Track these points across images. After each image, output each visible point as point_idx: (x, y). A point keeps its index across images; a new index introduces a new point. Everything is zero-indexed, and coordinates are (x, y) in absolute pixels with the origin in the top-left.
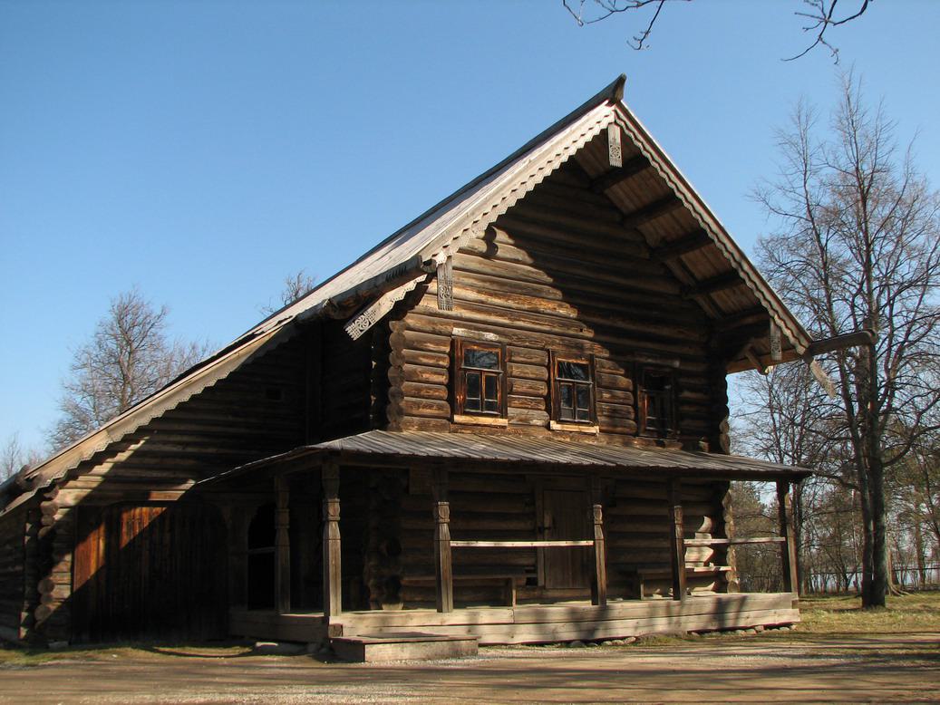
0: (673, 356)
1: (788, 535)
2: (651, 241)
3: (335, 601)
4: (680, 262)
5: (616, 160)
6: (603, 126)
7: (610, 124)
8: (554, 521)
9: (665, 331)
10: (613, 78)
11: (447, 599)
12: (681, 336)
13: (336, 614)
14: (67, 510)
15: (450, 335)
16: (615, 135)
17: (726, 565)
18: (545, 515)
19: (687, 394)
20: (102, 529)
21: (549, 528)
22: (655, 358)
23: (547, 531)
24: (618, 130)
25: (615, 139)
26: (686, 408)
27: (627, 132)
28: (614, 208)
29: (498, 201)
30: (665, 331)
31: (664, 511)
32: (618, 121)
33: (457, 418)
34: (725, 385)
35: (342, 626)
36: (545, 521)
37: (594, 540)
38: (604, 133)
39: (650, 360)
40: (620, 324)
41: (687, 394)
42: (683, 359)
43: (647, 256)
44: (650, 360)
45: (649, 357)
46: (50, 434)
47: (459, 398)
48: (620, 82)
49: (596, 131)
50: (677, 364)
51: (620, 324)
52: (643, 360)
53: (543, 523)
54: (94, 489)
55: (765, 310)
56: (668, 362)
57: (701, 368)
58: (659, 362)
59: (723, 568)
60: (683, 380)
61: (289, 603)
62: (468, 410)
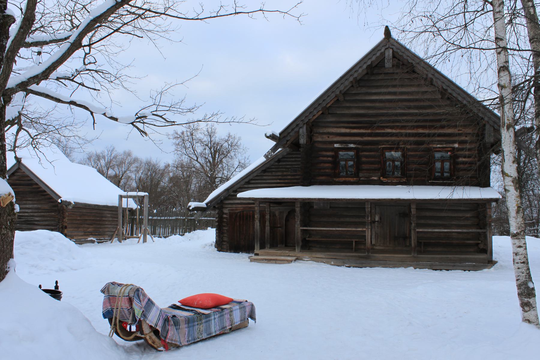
0: (454, 142)
6: (383, 50)
7: (386, 49)
8: (380, 218)
10: (383, 30)
12: (460, 132)
13: (257, 250)
14: (60, 80)
16: (389, 53)
18: (376, 216)
20: (6, 88)
21: (378, 221)
22: (441, 144)
23: (376, 222)
24: (391, 51)
26: (462, 166)
27: (395, 50)
31: (21, 211)
34: (15, 233)
36: (376, 218)
39: (438, 146)
40: (421, 131)
42: (460, 143)
43: (440, 96)
44: (438, 146)
45: (438, 144)
46: (515, 201)
48: (387, 32)
50: (456, 145)
51: (421, 131)
52: (435, 146)
53: (375, 219)
56: (451, 145)
58: (444, 146)
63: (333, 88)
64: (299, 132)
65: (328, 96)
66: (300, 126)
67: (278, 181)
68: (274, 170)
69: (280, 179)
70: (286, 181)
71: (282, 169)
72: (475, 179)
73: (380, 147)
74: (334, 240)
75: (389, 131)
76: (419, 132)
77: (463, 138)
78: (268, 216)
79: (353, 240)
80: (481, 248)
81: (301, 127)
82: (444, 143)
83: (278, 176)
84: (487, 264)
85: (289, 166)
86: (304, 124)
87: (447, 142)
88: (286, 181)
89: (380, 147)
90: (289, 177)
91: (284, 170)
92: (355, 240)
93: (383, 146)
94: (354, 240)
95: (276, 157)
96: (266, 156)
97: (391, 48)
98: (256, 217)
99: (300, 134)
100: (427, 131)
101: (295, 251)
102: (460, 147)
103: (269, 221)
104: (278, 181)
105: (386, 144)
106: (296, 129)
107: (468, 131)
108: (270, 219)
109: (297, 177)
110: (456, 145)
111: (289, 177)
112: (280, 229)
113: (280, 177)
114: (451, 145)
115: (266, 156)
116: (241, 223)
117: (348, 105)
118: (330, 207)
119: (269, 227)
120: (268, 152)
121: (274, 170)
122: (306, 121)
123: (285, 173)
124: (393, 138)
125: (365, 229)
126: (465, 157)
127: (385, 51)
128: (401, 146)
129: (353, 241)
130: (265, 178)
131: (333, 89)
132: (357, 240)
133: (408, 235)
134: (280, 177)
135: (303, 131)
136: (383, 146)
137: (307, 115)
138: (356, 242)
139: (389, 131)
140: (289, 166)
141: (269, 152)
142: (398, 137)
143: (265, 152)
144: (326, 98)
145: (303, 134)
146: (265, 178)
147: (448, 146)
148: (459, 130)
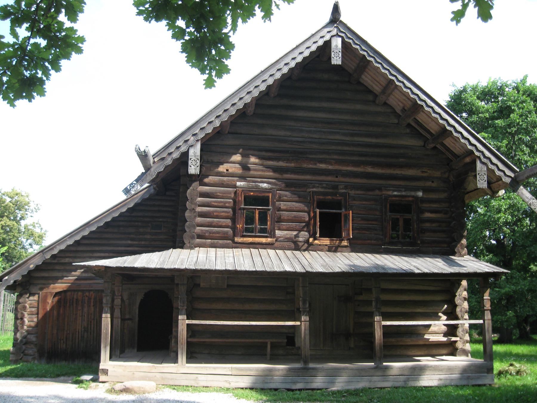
0: (417, 189)
1: (486, 318)
2: (398, 110)
3: (105, 354)
4: (417, 122)
5: (336, 60)
6: (327, 38)
9: (411, 172)
11: (182, 357)
12: (425, 175)
15: (235, 186)
16: (337, 43)
17: (456, 336)
19: (428, 215)
24: (340, 40)
25: (336, 46)
26: (427, 225)
28: (369, 91)
29: (236, 100)
30: (411, 172)
32: (340, 34)
33: (238, 239)
35: (108, 370)
37: (301, 322)
38: (327, 44)
39: (395, 193)
40: (370, 170)
41: (428, 215)
42: (425, 190)
44: (395, 193)
45: (394, 191)
47: (239, 226)
48: (336, 9)
49: (321, 43)
50: (420, 194)
51: (370, 170)
52: (390, 193)
54: (72, 283)
55: (472, 152)
56: (413, 193)
57: (443, 196)
58: (404, 193)
59: (454, 339)
60: (425, 205)
61: (119, 351)
62: (245, 234)
63: (250, 86)
64: (187, 153)
65: (241, 99)
66: (190, 143)
67: (129, 242)
68: (121, 223)
69: (132, 240)
70: (143, 243)
71: (137, 223)
72: (446, 245)
73: (309, 190)
74: (227, 340)
75: (323, 166)
76: (367, 171)
77: (428, 184)
78: (119, 300)
79: (267, 341)
80: (460, 348)
81: (192, 146)
82: (403, 189)
83: (130, 233)
84: (486, 374)
85: (148, 219)
86: (198, 141)
87: (407, 189)
88: (143, 243)
89: (309, 190)
90: (148, 237)
91: (140, 224)
92: (272, 340)
93: (314, 189)
94: (269, 342)
95: (131, 201)
96: (126, 191)
97: (340, 36)
98: (104, 301)
99: (190, 158)
100: (379, 171)
101: (177, 363)
102: (425, 196)
103: (121, 309)
104: (129, 242)
105: (318, 187)
106: (183, 149)
107: (438, 174)
108: (121, 306)
109: (162, 237)
110: (420, 194)
111: (148, 237)
112: (129, 322)
113: (132, 236)
114: (413, 193)
115: (126, 191)
116: (61, 311)
117: (260, 121)
118: (228, 286)
119: (120, 319)
120: (130, 185)
121: (121, 223)
122: (201, 136)
123: (141, 230)
124: (330, 178)
125: (298, 323)
126: (432, 212)
127: (331, 39)
128: (340, 191)
129: (267, 343)
130: (106, 236)
131: (249, 88)
132: (274, 340)
133: (351, 331)
134: (132, 236)
135: (195, 152)
136: (314, 189)
137: (203, 126)
138: (271, 343)
139: (323, 166)
140: (148, 219)
141: (132, 184)
142: (337, 177)
143: (126, 184)
144: (236, 101)
145: (194, 158)
146: (106, 236)
147: (409, 194)
148: (423, 172)
